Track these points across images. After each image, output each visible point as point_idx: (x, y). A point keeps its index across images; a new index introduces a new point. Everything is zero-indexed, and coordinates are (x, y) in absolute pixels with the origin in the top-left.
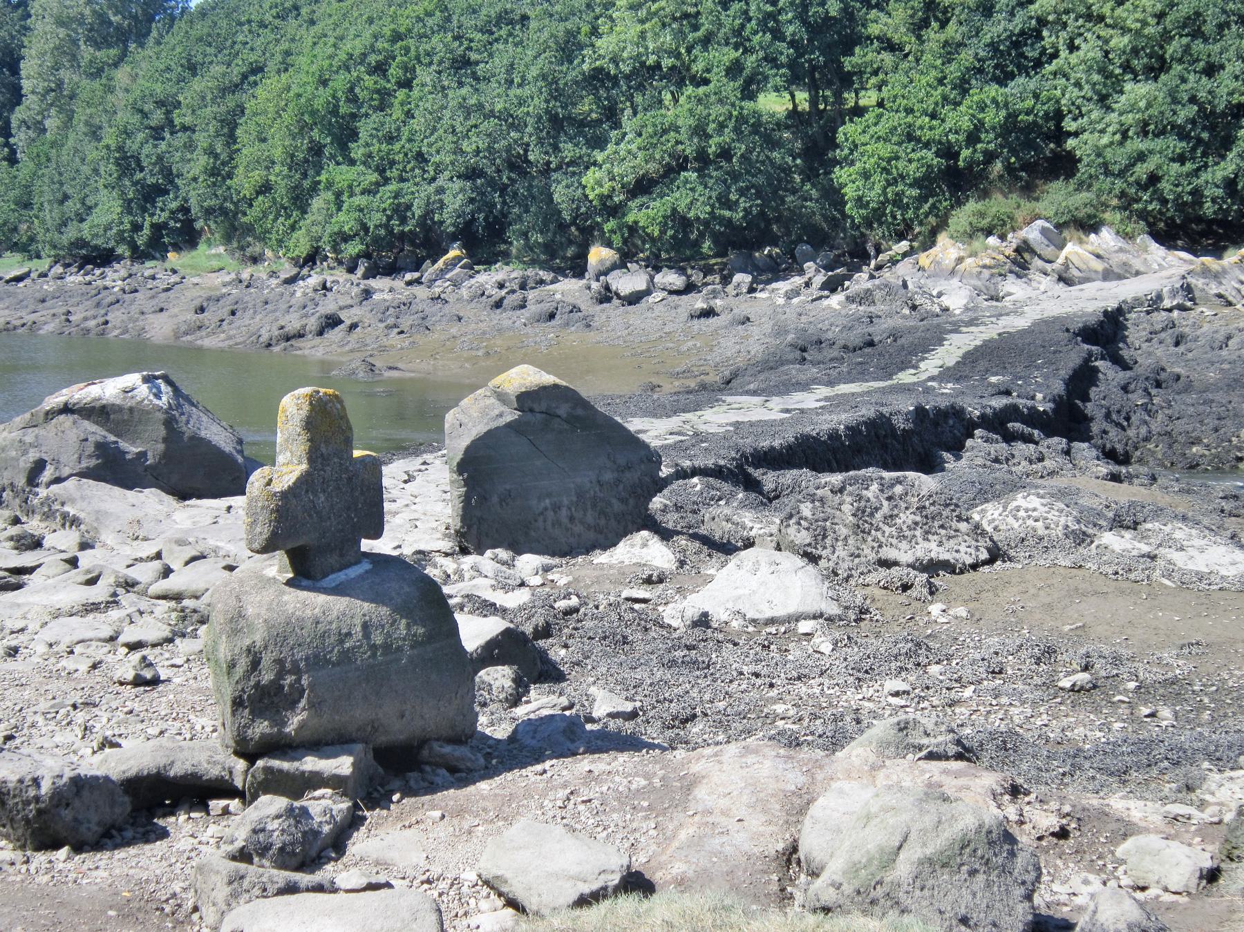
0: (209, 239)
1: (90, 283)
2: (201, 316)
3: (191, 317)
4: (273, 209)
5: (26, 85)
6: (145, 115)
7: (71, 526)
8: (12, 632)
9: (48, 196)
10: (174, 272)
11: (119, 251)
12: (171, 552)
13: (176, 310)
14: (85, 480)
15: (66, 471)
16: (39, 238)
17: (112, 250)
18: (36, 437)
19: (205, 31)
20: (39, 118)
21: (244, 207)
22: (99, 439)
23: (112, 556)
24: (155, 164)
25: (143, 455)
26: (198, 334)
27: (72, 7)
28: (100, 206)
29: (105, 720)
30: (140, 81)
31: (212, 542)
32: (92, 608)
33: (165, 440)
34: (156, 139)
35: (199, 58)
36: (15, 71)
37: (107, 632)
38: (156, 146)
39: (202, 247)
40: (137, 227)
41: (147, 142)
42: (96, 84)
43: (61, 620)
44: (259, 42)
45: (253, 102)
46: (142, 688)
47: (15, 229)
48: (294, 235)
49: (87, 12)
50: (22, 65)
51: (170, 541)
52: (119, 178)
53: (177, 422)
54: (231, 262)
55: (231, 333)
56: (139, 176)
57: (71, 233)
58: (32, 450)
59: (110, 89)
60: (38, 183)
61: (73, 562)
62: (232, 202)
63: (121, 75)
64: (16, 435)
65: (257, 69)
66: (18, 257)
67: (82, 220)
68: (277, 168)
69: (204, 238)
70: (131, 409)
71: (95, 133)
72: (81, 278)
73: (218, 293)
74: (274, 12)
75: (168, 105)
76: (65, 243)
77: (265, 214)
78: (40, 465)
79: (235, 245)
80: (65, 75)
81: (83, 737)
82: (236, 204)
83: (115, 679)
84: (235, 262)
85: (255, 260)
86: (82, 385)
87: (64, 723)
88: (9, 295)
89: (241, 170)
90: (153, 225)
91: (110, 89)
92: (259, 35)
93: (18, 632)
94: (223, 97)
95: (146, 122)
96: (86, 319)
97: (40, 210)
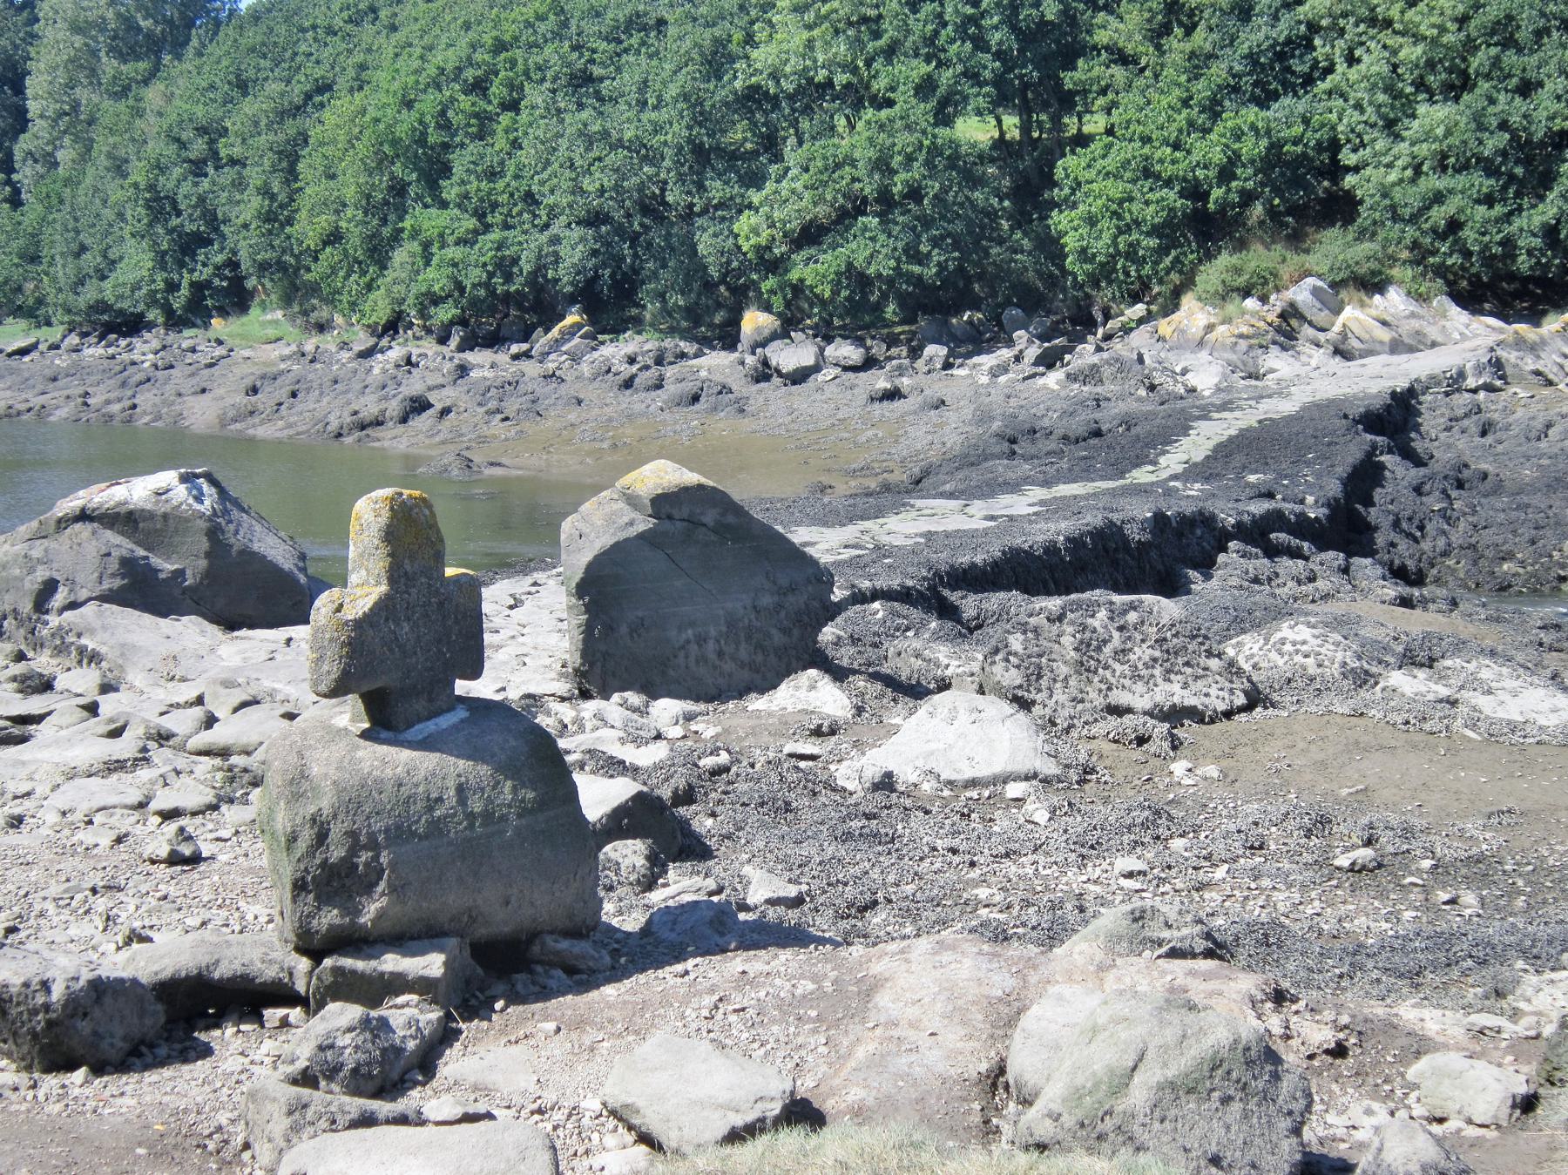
0: (263, 301)
1: (113, 357)
2: (253, 399)
3: (241, 399)
4: (344, 264)
5: (33, 107)
6: (183, 145)
7: (89, 663)
8: (16, 797)
9: (60, 247)
10: (220, 342)
11: (150, 316)
12: (216, 696)
13: (222, 391)
14: (107, 606)
15: (83, 594)
16: (49, 300)
17: (142, 315)
18: (46, 551)
19: (259, 39)
20: (49, 148)
21: (308, 261)
22: (125, 553)
23: (142, 701)
24: (195, 207)
25: (180, 573)
26: (250, 421)
27: (91, 9)
28: (126, 260)
29: (132, 908)
30: (177, 102)
31: (267, 684)
32: (115, 766)
33: (208, 555)
34: (197, 175)
35: (251, 73)
36: (19, 89)
37: (135, 797)
38: (196, 184)
39: (255, 311)
40: (172, 287)
41: (185, 179)
42: (121, 106)
43: (77, 781)
44: (326, 53)
45: (319, 128)
46: (179, 868)
47: (19, 289)
48: (371, 297)
49: (110, 15)
50: (28, 82)
51: (214, 682)
52: (150, 225)
53: (223, 532)
54: (291, 331)
55: (292, 419)
56: (175, 222)
57: (89, 294)
58: (40, 567)
59: (138, 113)
60: (48, 230)
61: (92, 709)
62: (292, 255)
63: (153, 95)
64: (20, 548)
65: (324, 87)
66: (23, 324)
67: (103, 278)
68: (349, 212)
69: (257, 300)
70: (165, 516)
71: (119, 168)
72: (102, 351)
73: (275, 370)
74: (345, 15)
75: (212, 132)
76: (83, 306)
77: (334, 270)
78: (50, 587)
79: (296, 308)
80: (83, 94)
81: (105, 930)
82: (297, 257)
83: (145, 856)
84: (297, 331)
85: (321, 328)
86: (103, 485)
87: (81, 911)
88: (12, 371)
89: (303, 214)
90: (192, 284)
91: (138, 113)
92: (326, 44)
93: (23, 797)
94: (281, 122)
95: (184, 154)
96: (108, 402)
97: (50, 265)
